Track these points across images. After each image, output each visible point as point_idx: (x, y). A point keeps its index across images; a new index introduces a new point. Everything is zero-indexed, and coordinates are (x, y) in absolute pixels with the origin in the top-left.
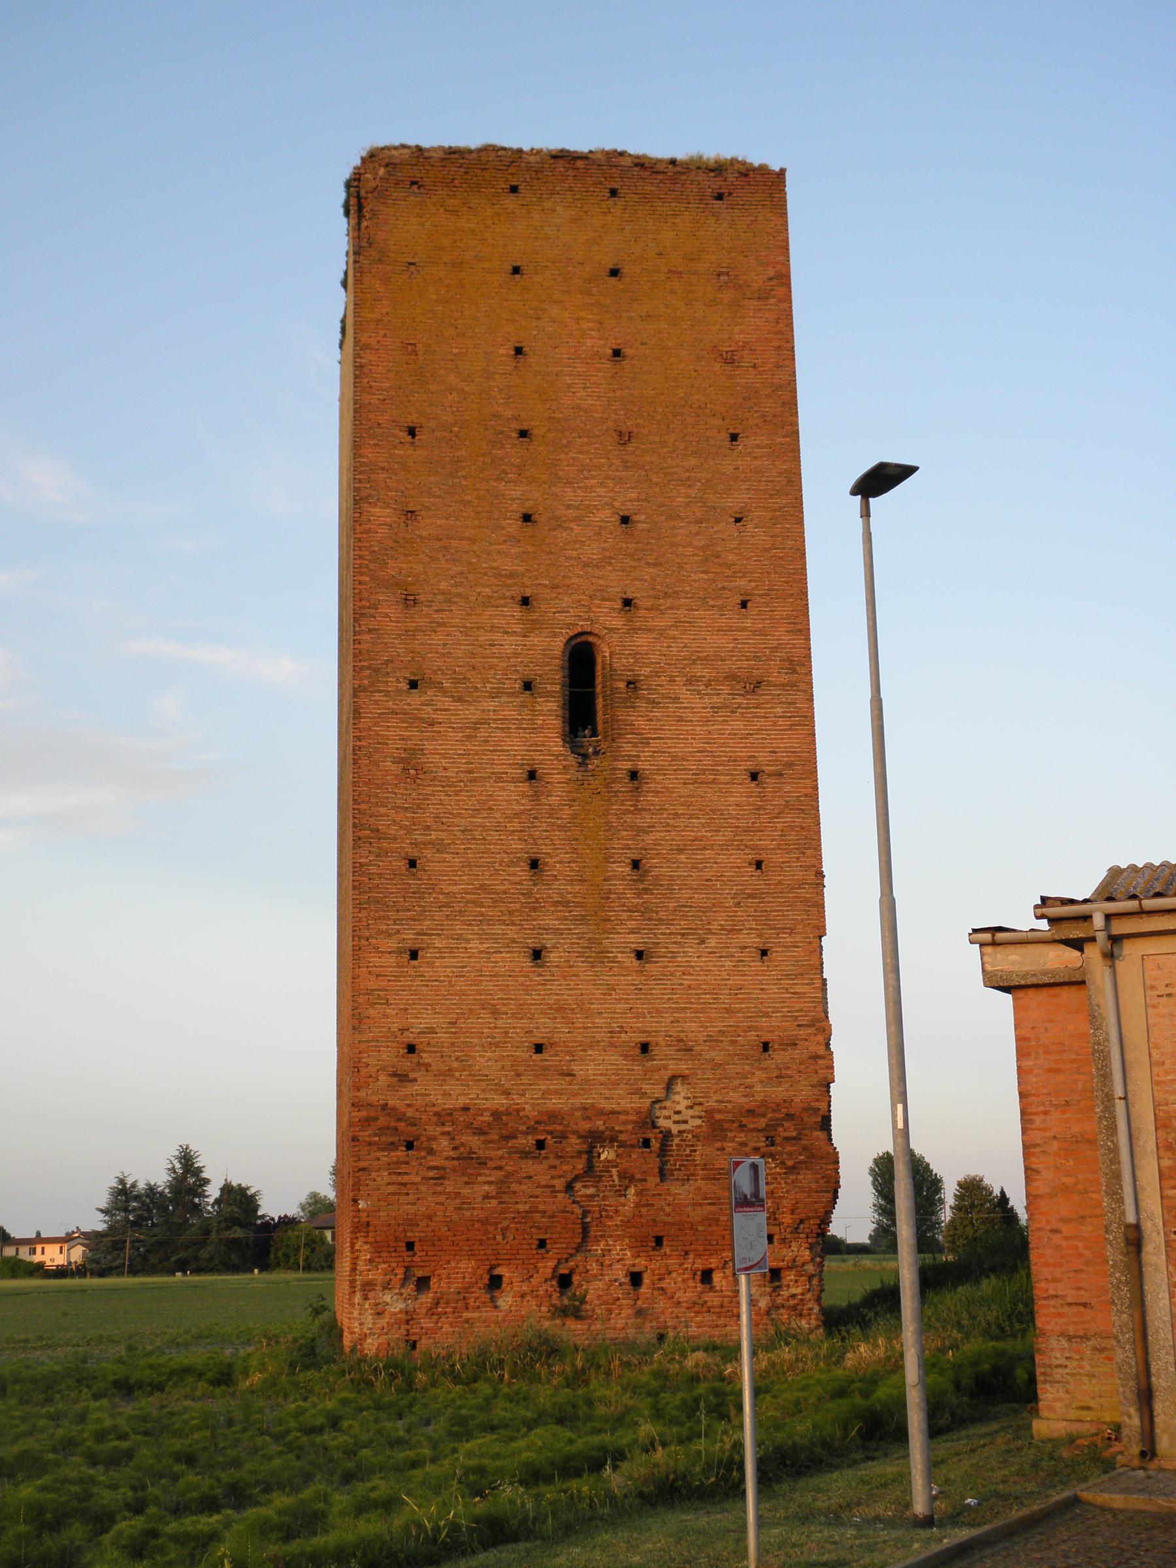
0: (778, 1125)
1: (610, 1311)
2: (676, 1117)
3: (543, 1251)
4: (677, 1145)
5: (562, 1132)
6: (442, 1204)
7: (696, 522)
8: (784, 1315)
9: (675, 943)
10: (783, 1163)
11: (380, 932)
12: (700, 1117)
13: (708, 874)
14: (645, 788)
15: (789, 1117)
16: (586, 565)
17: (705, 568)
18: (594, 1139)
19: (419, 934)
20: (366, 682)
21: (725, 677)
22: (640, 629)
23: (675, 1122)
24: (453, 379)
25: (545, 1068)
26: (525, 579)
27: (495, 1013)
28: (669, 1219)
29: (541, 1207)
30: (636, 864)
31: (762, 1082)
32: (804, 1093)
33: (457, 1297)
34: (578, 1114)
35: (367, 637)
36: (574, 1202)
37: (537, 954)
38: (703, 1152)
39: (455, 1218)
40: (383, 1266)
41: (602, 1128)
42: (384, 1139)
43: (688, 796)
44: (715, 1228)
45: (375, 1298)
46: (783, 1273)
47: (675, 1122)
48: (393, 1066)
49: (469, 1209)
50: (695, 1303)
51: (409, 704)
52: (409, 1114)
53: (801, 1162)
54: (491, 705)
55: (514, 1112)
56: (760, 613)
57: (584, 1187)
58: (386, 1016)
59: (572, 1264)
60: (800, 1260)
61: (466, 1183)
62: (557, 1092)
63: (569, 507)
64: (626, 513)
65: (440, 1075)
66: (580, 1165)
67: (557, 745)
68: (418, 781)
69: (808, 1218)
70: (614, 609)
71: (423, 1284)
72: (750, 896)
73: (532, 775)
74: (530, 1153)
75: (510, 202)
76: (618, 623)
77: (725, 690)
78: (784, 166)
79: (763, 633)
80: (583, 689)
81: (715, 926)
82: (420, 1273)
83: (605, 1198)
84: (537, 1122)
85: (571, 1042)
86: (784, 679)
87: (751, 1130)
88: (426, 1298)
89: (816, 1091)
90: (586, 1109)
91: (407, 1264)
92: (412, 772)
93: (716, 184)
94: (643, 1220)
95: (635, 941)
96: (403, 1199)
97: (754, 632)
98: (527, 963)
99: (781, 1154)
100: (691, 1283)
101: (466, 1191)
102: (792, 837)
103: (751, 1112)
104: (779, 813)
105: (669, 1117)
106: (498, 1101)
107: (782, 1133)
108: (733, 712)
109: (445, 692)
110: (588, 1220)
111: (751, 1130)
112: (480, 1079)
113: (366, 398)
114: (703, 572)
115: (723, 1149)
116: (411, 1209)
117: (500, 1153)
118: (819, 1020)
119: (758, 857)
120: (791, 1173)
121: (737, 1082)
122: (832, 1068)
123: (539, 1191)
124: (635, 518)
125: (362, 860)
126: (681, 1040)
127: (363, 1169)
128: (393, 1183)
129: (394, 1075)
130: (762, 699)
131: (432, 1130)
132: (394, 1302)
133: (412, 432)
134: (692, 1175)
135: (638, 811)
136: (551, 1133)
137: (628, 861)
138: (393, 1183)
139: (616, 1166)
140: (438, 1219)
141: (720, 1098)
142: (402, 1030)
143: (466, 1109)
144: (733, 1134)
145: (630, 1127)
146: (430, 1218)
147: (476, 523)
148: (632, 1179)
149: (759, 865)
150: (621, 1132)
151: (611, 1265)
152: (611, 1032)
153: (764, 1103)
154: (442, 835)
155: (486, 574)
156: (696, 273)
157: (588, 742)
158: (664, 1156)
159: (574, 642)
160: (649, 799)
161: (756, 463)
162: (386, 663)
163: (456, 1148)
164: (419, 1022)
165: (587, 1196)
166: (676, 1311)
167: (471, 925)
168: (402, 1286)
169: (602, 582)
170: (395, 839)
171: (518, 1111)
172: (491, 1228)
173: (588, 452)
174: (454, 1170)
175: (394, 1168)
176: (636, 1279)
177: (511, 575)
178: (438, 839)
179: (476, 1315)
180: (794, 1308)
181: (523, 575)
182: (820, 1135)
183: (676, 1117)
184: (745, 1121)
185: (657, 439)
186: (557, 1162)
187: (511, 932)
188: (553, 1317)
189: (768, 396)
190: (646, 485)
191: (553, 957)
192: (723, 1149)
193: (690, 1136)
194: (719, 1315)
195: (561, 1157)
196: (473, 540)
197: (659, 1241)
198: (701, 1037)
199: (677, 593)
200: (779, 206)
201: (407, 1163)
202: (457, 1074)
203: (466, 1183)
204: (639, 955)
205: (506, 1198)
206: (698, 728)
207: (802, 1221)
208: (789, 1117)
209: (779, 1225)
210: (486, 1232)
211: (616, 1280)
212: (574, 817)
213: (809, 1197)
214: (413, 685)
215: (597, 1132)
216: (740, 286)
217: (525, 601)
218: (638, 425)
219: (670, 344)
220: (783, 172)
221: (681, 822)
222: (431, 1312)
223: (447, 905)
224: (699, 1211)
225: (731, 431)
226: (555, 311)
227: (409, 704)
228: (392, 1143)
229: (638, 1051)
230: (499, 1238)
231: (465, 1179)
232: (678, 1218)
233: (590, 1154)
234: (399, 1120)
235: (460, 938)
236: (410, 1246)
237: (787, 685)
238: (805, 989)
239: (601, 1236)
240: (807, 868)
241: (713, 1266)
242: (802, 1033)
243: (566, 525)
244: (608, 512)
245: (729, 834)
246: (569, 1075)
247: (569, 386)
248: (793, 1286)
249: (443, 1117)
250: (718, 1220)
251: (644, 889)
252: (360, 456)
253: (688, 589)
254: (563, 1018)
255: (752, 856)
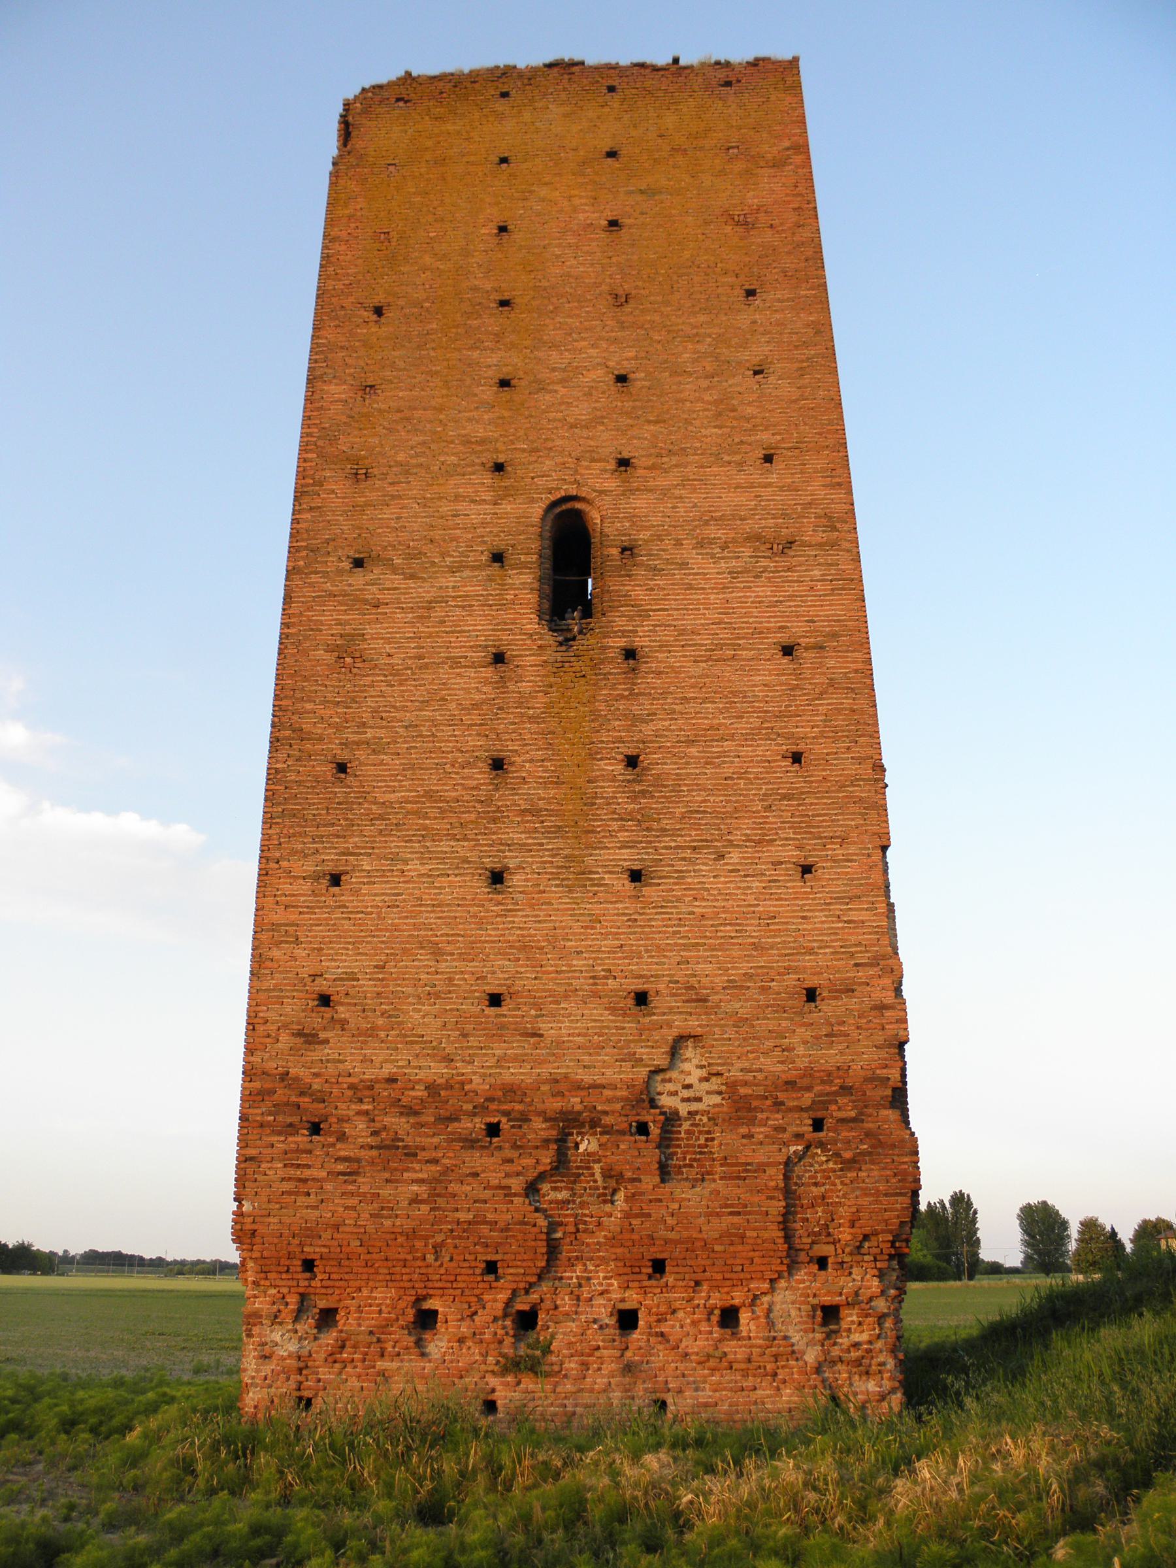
0: (830, 1102)
1: (585, 1365)
2: (686, 1094)
3: (491, 1277)
4: (687, 1132)
5: (522, 1113)
6: (354, 1208)
7: (707, 377)
8: (842, 1373)
9: (684, 859)
10: (837, 1155)
11: (294, 852)
12: (720, 1093)
13: (728, 771)
14: (644, 668)
15: (845, 1090)
16: (573, 426)
17: (718, 423)
18: (568, 1125)
19: (344, 854)
20: (301, 563)
21: (747, 538)
22: (638, 490)
23: (684, 1100)
24: (428, 260)
25: (502, 1026)
26: (498, 445)
27: (437, 953)
28: (672, 1235)
29: (490, 1216)
30: (632, 762)
31: (805, 1042)
32: (865, 1058)
33: (368, 1339)
34: (545, 1088)
35: (308, 516)
36: (537, 1210)
37: (497, 878)
38: (725, 1140)
39: (371, 1228)
40: (273, 1291)
41: (578, 1107)
42: (280, 1118)
43: (699, 677)
44: (740, 1248)
45: (260, 1335)
46: (844, 1312)
47: (684, 1100)
48: (299, 1023)
49: (390, 1217)
50: (709, 1356)
51: (350, 585)
52: (315, 1087)
53: (862, 1154)
54: (450, 581)
55: (459, 1086)
56: (787, 467)
57: (554, 1189)
58: (294, 958)
59: (534, 1297)
60: (865, 1294)
61: (387, 1181)
62: (519, 1060)
63: (554, 370)
64: (623, 372)
65: (360, 1035)
66: (547, 1158)
67: (530, 622)
68: (355, 671)
69: (876, 1233)
70: (606, 471)
71: (327, 1318)
72: (785, 797)
73: (499, 658)
74: (478, 1141)
75: (501, 106)
76: (611, 484)
77: (747, 552)
78: (796, 55)
79: (793, 488)
80: (569, 562)
81: (737, 837)
82: (322, 1304)
83: (583, 1205)
84: (490, 1099)
85: (537, 991)
86: (821, 537)
87: (790, 1110)
88: (329, 1338)
89: (883, 1054)
90: (557, 1081)
91: (301, 1290)
92: (348, 660)
93: (721, 75)
94: (635, 1237)
95: (629, 858)
96: (301, 1200)
97: (781, 489)
98: (481, 887)
99: (835, 1142)
100: (704, 1327)
101: (386, 1192)
102: (840, 721)
103: (790, 1084)
104: (821, 694)
105: (675, 1093)
106: (436, 1071)
107: (835, 1112)
108: (756, 577)
109: (394, 570)
110: (559, 1235)
111: (790, 1110)
112: (415, 1042)
113: (330, 284)
114: (715, 427)
115: (750, 1136)
116: (313, 1214)
117: (435, 1140)
118: (884, 957)
119: (794, 748)
120: (849, 1169)
121: (770, 1044)
122: (906, 1021)
123: (488, 1194)
124: (632, 376)
125: (278, 766)
126: (692, 988)
127: (252, 1159)
128: (290, 1179)
129: (299, 1034)
130: (794, 561)
131: (346, 1108)
132: (285, 1341)
133: (379, 311)
134: (708, 1173)
135: (633, 695)
136: (506, 1114)
137: (620, 757)
138: (290, 1179)
139: (599, 1161)
140: (347, 1229)
141: (746, 1065)
142: (314, 976)
143: (392, 1080)
144: (764, 1115)
145: (618, 1106)
146: (337, 1227)
147: (444, 392)
148: (620, 1178)
149: (797, 758)
150: (606, 1113)
151: (591, 1299)
152: (594, 977)
153: (808, 1072)
154: (380, 733)
155: (452, 442)
156: (702, 148)
157: (574, 621)
158: (668, 1147)
159: (558, 510)
160: (647, 681)
161: (777, 316)
162: (328, 542)
163: (375, 1133)
164: (333, 968)
165: (557, 1202)
166: (682, 1366)
167: (411, 840)
168: (296, 1320)
169: (592, 443)
170: (321, 739)
171: (462, 1084)
172: (419, 1244)
173: (578, 316)
174: (372, 1162)
175: (291, 1159)
176: (627, 1320)
177: (482, 442)
178: (375, 738)
179: (394, 1365)
180: (858, 1362)
181: (497, 440)
182: (893, 1115)
183: (686, 1094)
184: (782, 1096)
185: (659, 298)
186: (514, 1154)
187: (463, 849)
188: (505, 1371)
189: (789, 253)
190: (646, 343)
191: (516, 880)
192: (750, 1136)
193: (705, 1119)
194: (745, 1375)
195: (520, 1147)
196: (440, 409)
197: (659, 1267)
198: (720, 982)
199: (684, 449)
200: (795, 89)
201: (310, 1152)
202: (382, 1034)
203: (387, 1181)
204: (636, 876)
205: (441, 1202)
206: (712, 597)
207: (866, 1237)
208: (845, 1090)
209: (834, 1243)
210: (412, 1249)
211: (595, 1321)
212: (550, 705)
213: (877, 1202)
214: (358, 563)
215: (571, 1112)
216: (752, 157)
217: (499, 468)
218: (636, 287)
219: (673, 212)
220: (795, 61)
221: (691, 708)
222: (332, 1358)
223: (381, 817)
224: (715, 1221)
225: (747, 287)
226: (543, 192)
227: (350, 585)
228: (291, 1125)
229: (630, 1002)
230: (430, 1258)
231: (387, 1175)
232: (685, 1234)
233: (562, 1144)
234: (302, 1094)
235: (395, 858)
236: (309, 1265)
237: (825, 544)
238: (864, 915)
239: (577, 1258)
240: (861, 760)
241: (736, 1302)
242: (861, 974)
243: (551, 387)
244: (600, 372)
245: (756, 722)
246: (534, 1035)
247: (557, 257)
248: (856, 1331)
249: (361, 1090)
250: (743, 1237)
251: (639, 792)
252: (318, 337)
253: (698, 445)
254: (528, 959)
255: (787, 747)
